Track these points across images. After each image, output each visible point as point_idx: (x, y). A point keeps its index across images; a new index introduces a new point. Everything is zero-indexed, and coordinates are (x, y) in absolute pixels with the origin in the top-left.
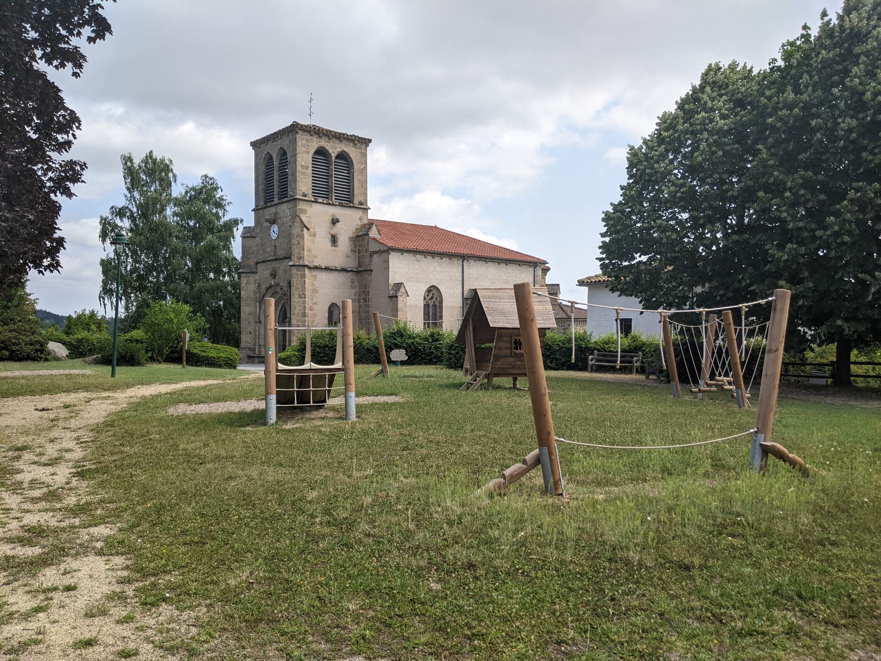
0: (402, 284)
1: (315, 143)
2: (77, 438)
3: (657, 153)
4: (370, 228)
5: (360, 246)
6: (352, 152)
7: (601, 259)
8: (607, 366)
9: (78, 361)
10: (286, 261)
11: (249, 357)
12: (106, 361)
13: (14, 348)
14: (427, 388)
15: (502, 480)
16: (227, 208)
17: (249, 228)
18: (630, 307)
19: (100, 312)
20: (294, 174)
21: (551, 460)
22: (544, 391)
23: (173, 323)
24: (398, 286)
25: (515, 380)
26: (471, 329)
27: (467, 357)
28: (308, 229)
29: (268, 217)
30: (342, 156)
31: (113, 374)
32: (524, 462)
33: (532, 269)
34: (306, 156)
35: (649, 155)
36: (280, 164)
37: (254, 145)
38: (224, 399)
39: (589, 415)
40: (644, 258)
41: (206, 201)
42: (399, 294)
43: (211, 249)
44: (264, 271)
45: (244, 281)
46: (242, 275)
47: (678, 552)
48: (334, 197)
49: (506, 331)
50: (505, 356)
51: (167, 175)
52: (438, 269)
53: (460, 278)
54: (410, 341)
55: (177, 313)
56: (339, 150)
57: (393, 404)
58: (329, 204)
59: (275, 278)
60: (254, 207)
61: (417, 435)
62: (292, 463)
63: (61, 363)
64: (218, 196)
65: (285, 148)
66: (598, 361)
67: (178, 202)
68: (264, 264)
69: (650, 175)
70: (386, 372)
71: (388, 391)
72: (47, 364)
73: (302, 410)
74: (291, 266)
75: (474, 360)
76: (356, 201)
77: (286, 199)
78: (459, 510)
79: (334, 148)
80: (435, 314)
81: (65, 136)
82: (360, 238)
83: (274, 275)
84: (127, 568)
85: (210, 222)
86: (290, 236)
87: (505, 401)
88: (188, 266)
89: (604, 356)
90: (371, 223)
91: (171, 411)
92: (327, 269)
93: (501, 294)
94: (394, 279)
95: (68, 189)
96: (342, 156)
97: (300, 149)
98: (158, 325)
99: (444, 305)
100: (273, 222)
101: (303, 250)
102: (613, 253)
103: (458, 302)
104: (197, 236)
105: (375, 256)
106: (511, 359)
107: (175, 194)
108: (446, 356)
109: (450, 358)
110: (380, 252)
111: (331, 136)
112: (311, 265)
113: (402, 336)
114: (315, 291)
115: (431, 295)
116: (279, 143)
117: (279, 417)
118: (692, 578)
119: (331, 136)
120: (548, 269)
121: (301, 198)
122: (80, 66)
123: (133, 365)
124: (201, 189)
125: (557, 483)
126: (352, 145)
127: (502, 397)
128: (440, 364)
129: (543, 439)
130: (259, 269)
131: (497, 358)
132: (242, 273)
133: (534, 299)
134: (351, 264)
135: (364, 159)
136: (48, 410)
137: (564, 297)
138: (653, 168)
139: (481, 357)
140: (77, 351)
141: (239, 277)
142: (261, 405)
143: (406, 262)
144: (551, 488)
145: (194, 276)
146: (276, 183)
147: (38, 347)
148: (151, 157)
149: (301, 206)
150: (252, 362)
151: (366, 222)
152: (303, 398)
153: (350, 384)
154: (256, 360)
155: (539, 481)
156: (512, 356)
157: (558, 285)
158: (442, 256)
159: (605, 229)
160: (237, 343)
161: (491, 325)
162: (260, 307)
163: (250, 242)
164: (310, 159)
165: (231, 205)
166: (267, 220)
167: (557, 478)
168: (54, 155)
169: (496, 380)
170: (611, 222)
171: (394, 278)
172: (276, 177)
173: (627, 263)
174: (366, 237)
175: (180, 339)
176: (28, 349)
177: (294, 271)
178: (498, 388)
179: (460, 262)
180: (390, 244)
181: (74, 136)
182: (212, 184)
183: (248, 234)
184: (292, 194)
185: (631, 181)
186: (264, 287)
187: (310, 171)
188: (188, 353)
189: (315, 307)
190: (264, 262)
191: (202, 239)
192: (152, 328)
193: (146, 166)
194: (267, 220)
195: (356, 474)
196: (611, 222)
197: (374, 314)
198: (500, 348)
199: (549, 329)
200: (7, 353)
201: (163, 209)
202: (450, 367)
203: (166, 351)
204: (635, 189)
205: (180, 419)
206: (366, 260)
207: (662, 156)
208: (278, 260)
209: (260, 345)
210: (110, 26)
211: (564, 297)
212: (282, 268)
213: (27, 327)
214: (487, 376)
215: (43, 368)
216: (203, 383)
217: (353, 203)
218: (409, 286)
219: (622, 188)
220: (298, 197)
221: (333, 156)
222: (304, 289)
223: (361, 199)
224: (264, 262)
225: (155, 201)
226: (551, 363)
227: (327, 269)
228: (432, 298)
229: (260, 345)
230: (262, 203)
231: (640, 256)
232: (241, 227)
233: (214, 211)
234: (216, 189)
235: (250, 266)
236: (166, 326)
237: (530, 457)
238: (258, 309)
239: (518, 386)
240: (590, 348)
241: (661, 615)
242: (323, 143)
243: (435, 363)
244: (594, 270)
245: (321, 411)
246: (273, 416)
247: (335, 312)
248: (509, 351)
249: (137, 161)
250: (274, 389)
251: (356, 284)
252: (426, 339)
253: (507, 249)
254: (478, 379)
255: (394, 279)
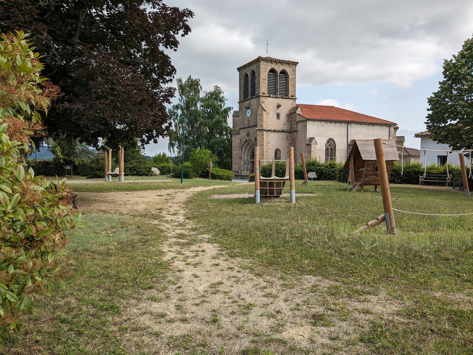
0: (313, 138)
1: (270, 66)
2: (179, 206)
3: (460, 63)
4: (297, 109)
5: (291, 118)
6: (288, 69)
7: (427, 123)
8: (430, 182)
9: (164, 176)
10: (254, 128)
11: (236, 176)
12: (177, 176)
13: (138, 170)
14: (329, 190)
15: (367, 227)
16: (225, 102)
17: (236, 111)
18: (444, 149)
19: (168, 154)
20: (259, 83)
21: (390, 219)
22: (387, 187)
23: (203, 159)
24: (312, 139)
25: (376, 187)
26: (352, 161)
27: (350, 175)
28: (265, 111)
29: (245, 106)
30: (283, 72)
31: (182, 182)
32: (378, 219)
33: (388, 128)
34: (265, 73)
35: (456, 65)
36: (252, 78)
37: (239, 69)
38: (234, 193)
39: (414, 204)
40: (454, 122)
41: (216, 99)
42: (312, 143)
43: (218, 122)
44: (243, 133)
45: (234, 138)
46: (233, 135)
47: (446, 254)
48: (278, 94)
49: (371, 162)
50: (371, 175)
51: (197, 87)
52: (334, 129)
53: (346, 134)
54: (318, 168)
55: (205, 154)
56: (282, 69)
57: (312, 197)
58: (276, 97)
59: (249, 136)
60: (238, 101)
61: (326, 209)
62: (271, 217)
63: (158, 177)
64: (221, 96)
65: (254, 70)
66: (425, 179)
67: (202, 100)
68: (243, 130)
69: (456, 76)
70: (307, 183)
71: (309, 192)
72: (152, 177)
73: (270, 197)
74: (257, 130)
75: (354, 178)
76: (290, 95)
77: (254, 96)
78: (347, 236)
79: (279, 68)
80: (331, 154)
81: (170, 77)
82: (292, 114)
83: (248, 135)
84: (220, 247)
85: (218, 109)
86: (256, 115)
87: (370, 197)
88: (207, 131)
89: (429, 176)
90: (297, 106)
91: (213, 197)
92: (274, 131)
93: (369, 143)
94: (309, 135)
95: (169, 100)
96: (283, 72)
97: (262, 70)
98: (197, 160)
99: (337, 148)
100: (248, 108)
101: (263, 122)
102: (434, 120)
103: (344, 147)
104: (210, 116)
105: (300, 123)
106: (374, 176)
107: (201, 97)
108: (338, 176)
109: (340, 177)
110: (302, 121)
111: (277, 62)
112: (267, 129)
113: (314, 165)
114: (268, 142)
115: (329, 143)
116: (251, 68)
117: (261, 201)
118: (450, 263)
119: (277, 62)
120: (398, 128)
121: (262, 95)
122: (177, 47)
123: (188, 178)
124: (214, 93)
125: (392, 229)
126: (288, 66)
127: (369, 195)
128: (334, 180)
129: (387, 209)
130: (241, 132)
131: (366, 176)
132: (233, 134)
133: (383, 146)
134: (286, 128)
135: (294, 73)
136: (161, 196)
137: (407, 144)
138: (457, 72)
139: (357, 177)
140: (163, 172)
141: (231, 137)
142: (252, 196)
143: (316, 126)
144: (390, 231)
145: (210, 136)
146: (250, 88)
147: (148, 169)
148: (190, 79)
149: (262, 99)
150: (238, 179)
151: (294, 105)
152: (271, 192)
153: (292, 186)
154: (239, 177)
155: (384, 228)
156: (374, 175)
157: (404, 137)
158: (336, 122)
159: (429, 107)
160: (230, 168)
161: (363, 159)
162: (241, 151)
163: (237, 119)
164: (267, 75)
165: (227, 101)
166: (245, 107)
167: (393, 227)
168: (162, 85)
169: (366, 187)
170: (433, 103)
171: (309, 135)
172: (250, 85)
173: (443, 125)
174: (295, 114)
175: (207, 166)
176: (144, 171)
177: (258, 132)
178: (366, 191)
179: (346, 125)
180: (308, 117)
181: (173, 77)
182: (219, 90)
183: (236, 115)
184: (257, 93)
185: (445, 79)
186: (243, 141)
187: (267, 81)
188: (212, 174)
189: (268, 150)
190: (243, 128)
191: (214, 118)
192: (193, 161)
193: (188, 83)
194: (245, 107)
195: (300, 222)
196: (433, 103)
197: (301, 154)
198: (368, 171)
199: (395, 161)
200: (135, 172)
201: (196, 105)
202: (340, 181)
203: (200, 172)
204: (447, 84)
205: (218, 200)
206: (294, 126)
207: (464, 65)
208: (250, 127)
209: (241, 170)
210: (190, 29)
211: (407, 144)
212: (252, 131)
213: (143, 161)
214: (361, 185)
215: (151, 179)
216: (221, 187)
217: (288, 96)
218: (317, 139)
219: (440, 83)
220: (260, 95)
221: (279, 72)
222: (263, 142)
223: (293, 94)
224: (243, 128)
225: (193, 100)
226: (398, 180)
227: (274, 131)
228: (330, 145)
229: (241, 170)
230: (242, 99)
231: (450, 121)
232: (232, 111)
233: (219, 104)
234: (220, 93)
235: (237, 131)
236: (200, 160)
237: (380, 217)
238: (240, 152)
239: (377, 191)
240: (421, 172)
241: (432, 273)
242: (274, 66)
243: (332, 180)
244: (423, 129)
245: (278, 199)
246: (258, 200)
247: (278, 153)
248: (372, 172)
249: (184, 82)
250: (259, 187)
251: (289, 138)
252: (327, 167)
253: (373, 117)
254: (356, 187)
255: (309, 135)
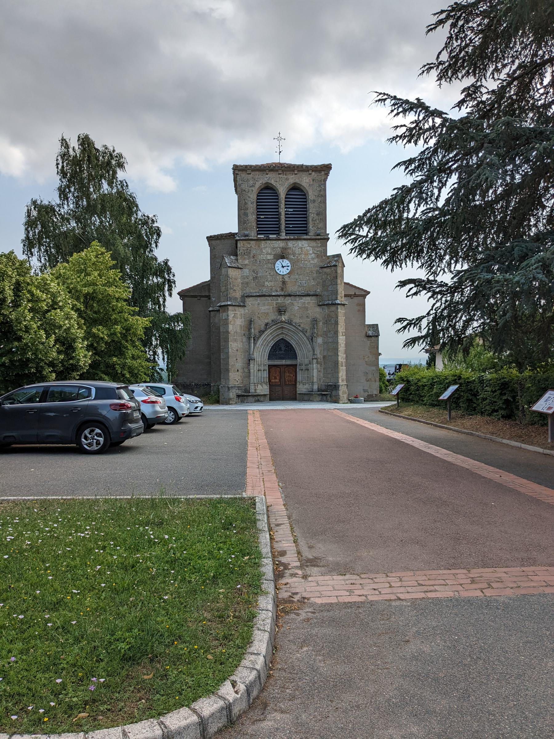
83: (281, 311)
